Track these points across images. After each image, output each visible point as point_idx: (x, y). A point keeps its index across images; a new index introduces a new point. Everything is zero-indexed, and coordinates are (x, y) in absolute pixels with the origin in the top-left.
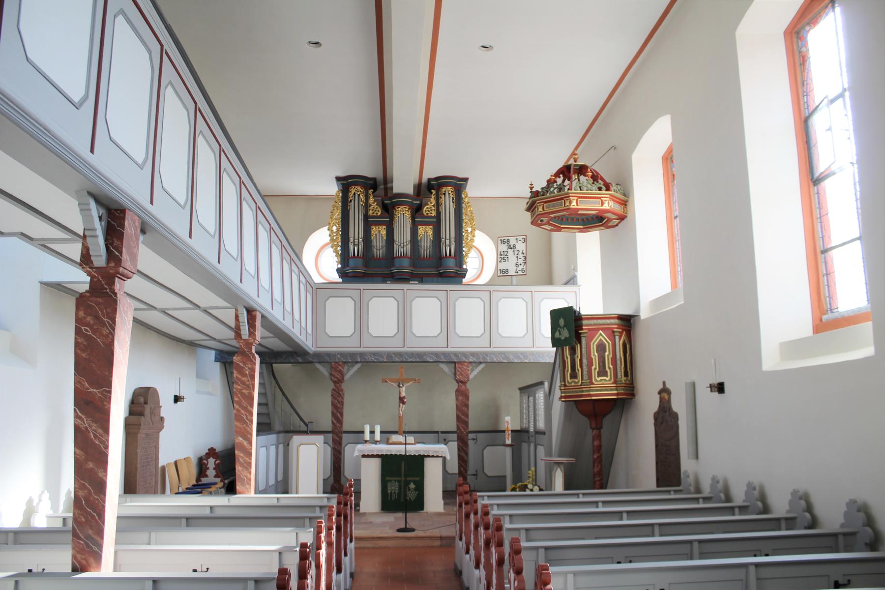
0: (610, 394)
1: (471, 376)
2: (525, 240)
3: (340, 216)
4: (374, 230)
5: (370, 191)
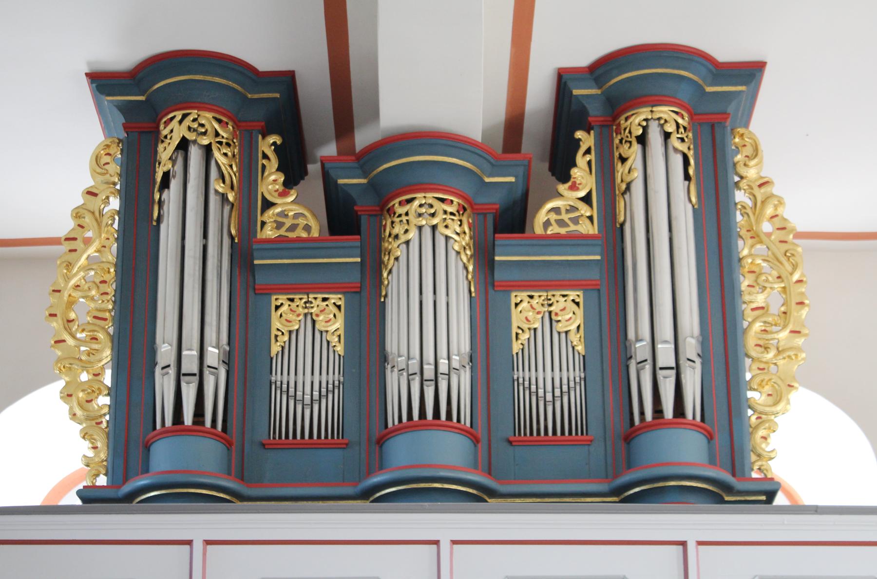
3: (111, 255)
4: (285, 316)
5: (268, 144)
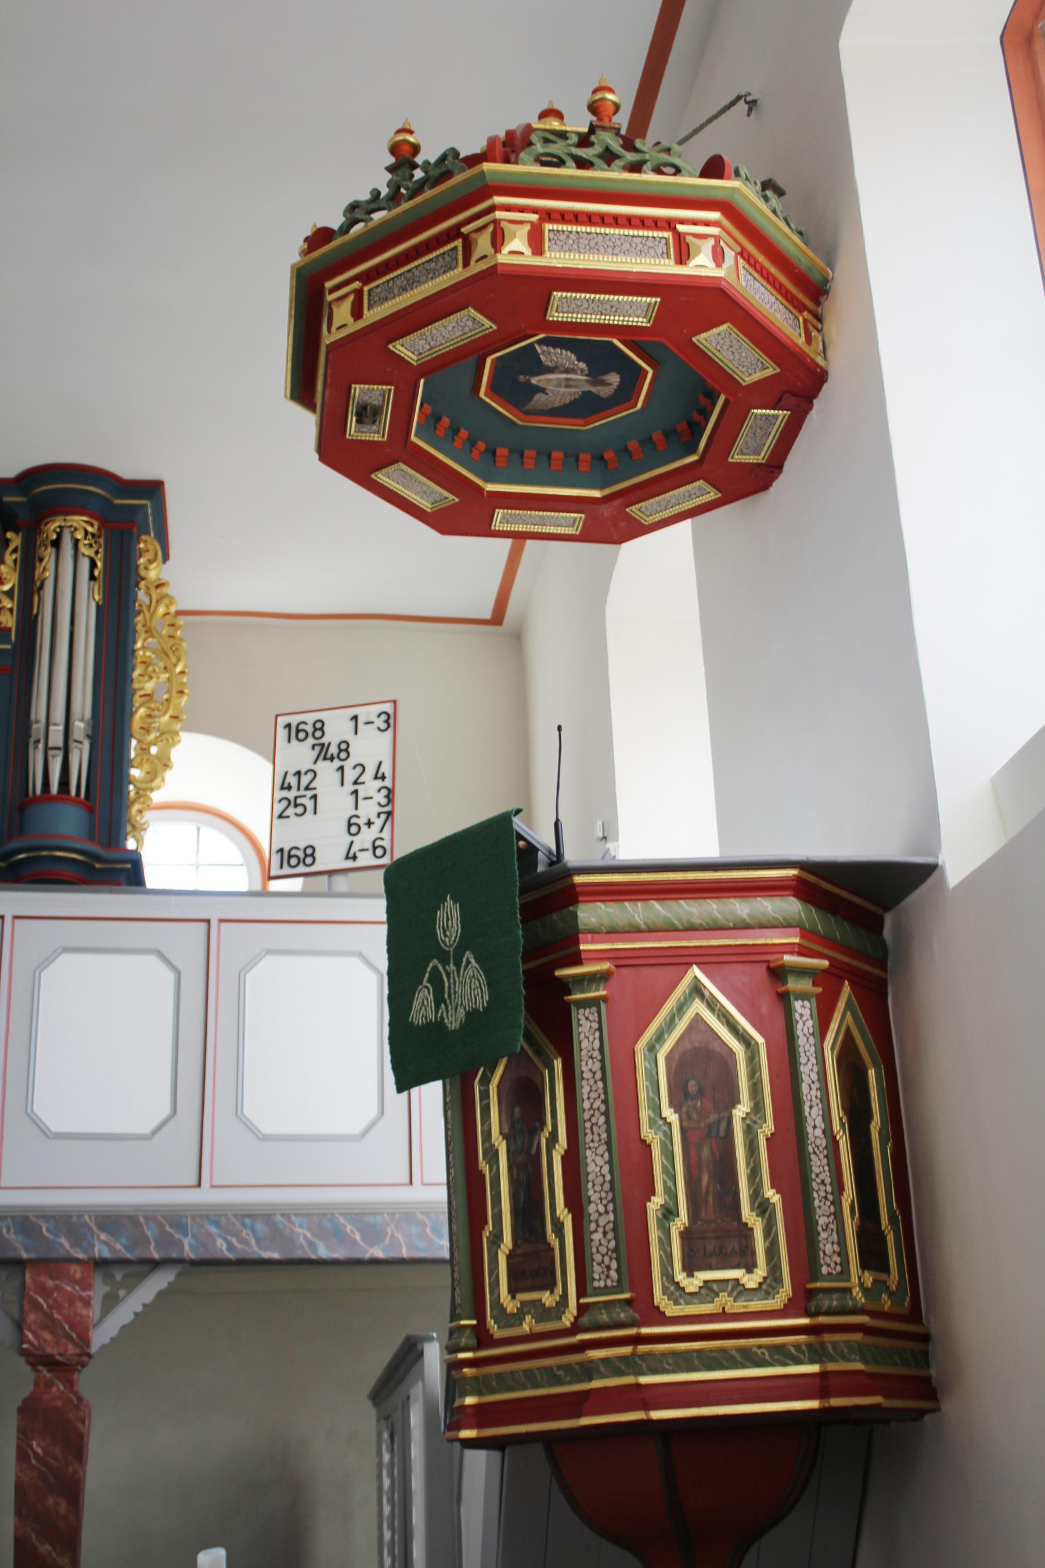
0: (772, 1383)
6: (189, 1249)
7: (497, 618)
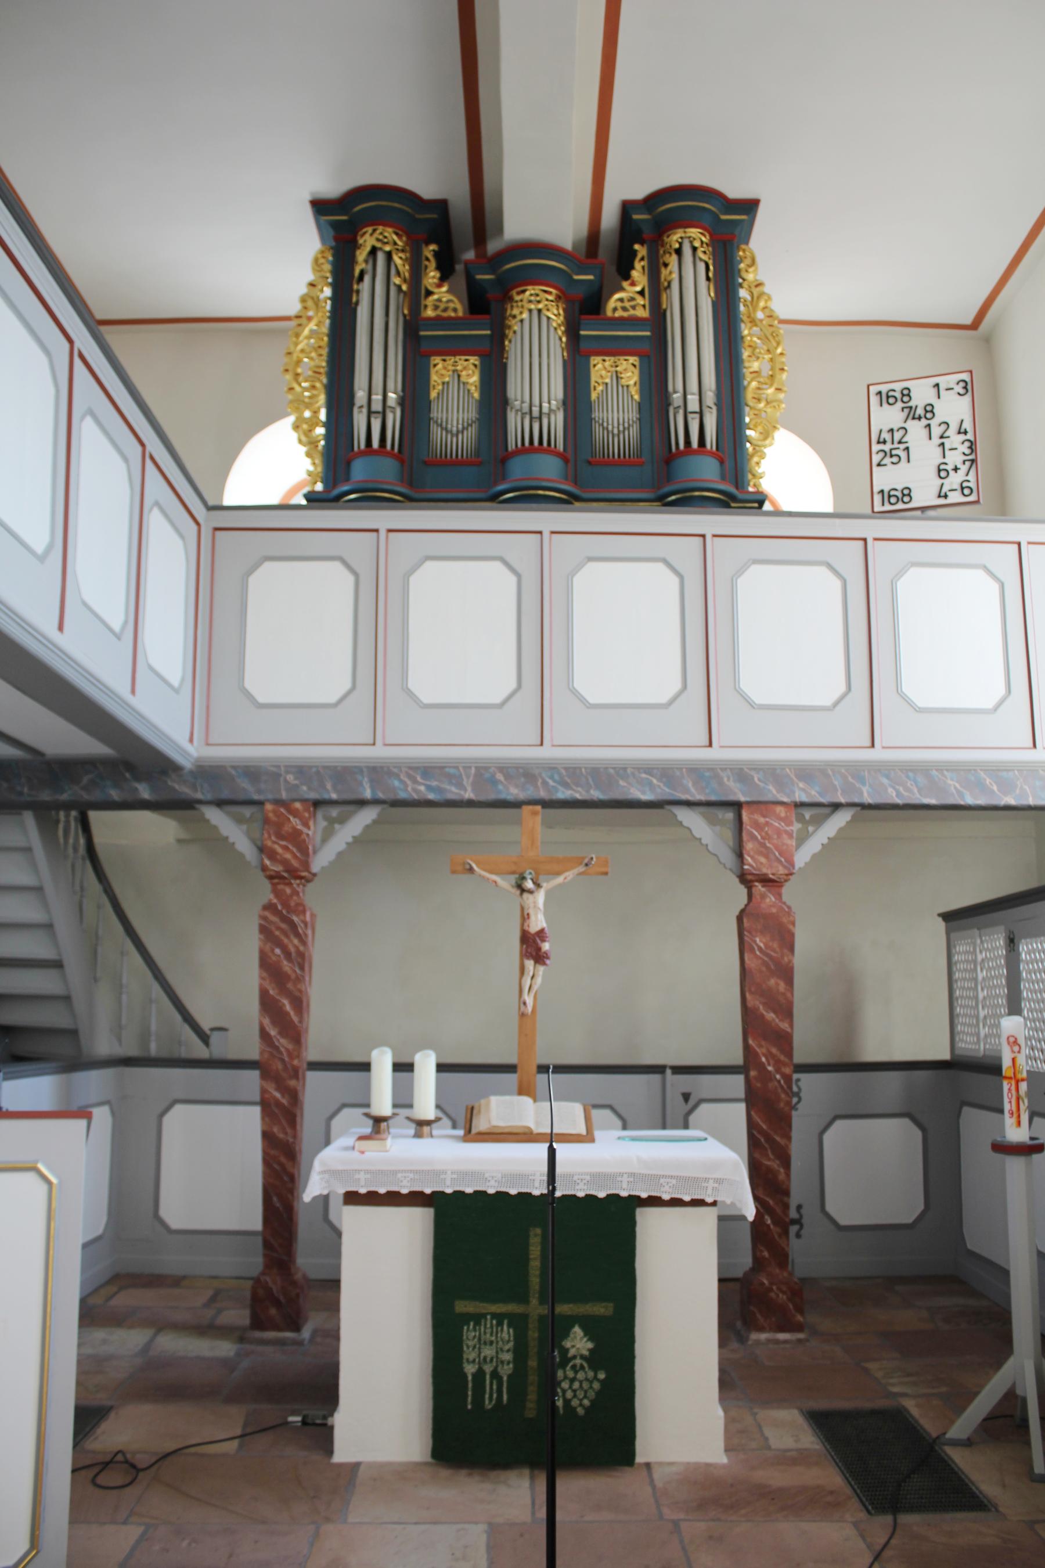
1: (802, 858)
2: (967, 387)
4: (440, 371)
6: (867, 797)
7: (975, 325)
